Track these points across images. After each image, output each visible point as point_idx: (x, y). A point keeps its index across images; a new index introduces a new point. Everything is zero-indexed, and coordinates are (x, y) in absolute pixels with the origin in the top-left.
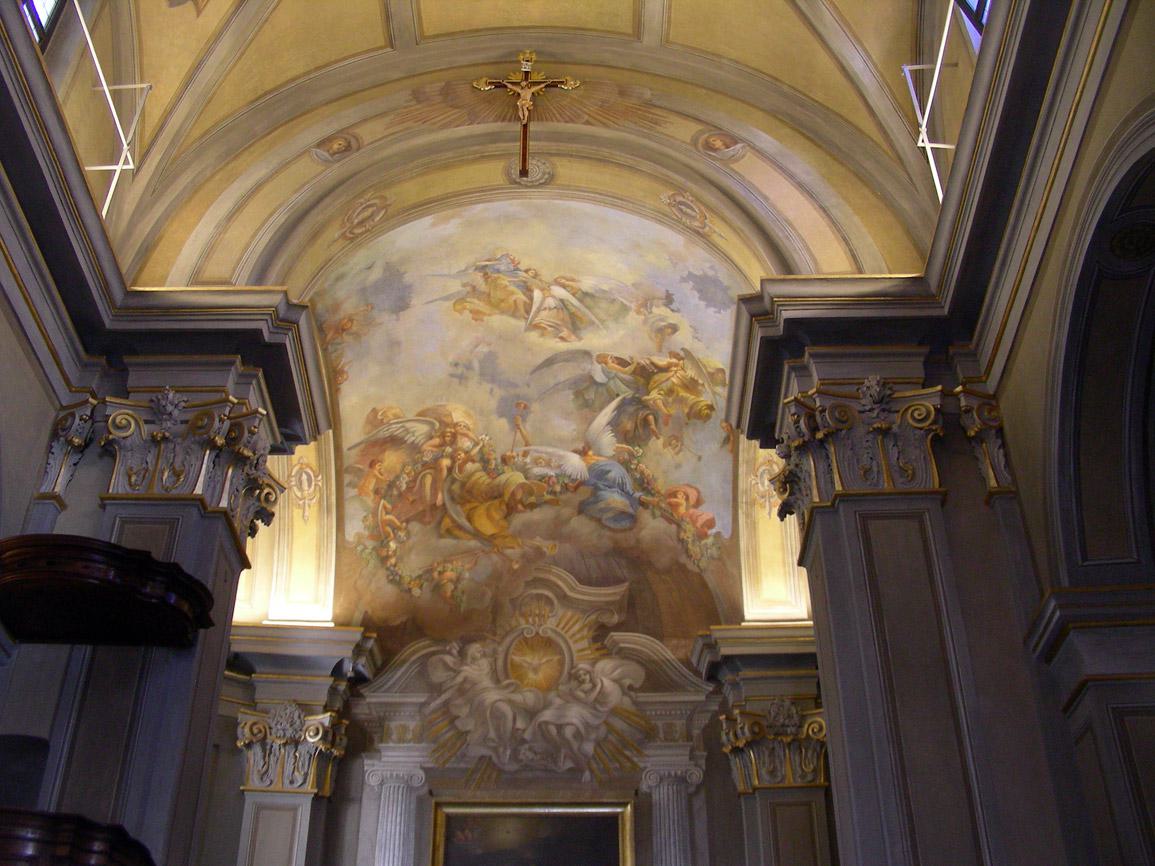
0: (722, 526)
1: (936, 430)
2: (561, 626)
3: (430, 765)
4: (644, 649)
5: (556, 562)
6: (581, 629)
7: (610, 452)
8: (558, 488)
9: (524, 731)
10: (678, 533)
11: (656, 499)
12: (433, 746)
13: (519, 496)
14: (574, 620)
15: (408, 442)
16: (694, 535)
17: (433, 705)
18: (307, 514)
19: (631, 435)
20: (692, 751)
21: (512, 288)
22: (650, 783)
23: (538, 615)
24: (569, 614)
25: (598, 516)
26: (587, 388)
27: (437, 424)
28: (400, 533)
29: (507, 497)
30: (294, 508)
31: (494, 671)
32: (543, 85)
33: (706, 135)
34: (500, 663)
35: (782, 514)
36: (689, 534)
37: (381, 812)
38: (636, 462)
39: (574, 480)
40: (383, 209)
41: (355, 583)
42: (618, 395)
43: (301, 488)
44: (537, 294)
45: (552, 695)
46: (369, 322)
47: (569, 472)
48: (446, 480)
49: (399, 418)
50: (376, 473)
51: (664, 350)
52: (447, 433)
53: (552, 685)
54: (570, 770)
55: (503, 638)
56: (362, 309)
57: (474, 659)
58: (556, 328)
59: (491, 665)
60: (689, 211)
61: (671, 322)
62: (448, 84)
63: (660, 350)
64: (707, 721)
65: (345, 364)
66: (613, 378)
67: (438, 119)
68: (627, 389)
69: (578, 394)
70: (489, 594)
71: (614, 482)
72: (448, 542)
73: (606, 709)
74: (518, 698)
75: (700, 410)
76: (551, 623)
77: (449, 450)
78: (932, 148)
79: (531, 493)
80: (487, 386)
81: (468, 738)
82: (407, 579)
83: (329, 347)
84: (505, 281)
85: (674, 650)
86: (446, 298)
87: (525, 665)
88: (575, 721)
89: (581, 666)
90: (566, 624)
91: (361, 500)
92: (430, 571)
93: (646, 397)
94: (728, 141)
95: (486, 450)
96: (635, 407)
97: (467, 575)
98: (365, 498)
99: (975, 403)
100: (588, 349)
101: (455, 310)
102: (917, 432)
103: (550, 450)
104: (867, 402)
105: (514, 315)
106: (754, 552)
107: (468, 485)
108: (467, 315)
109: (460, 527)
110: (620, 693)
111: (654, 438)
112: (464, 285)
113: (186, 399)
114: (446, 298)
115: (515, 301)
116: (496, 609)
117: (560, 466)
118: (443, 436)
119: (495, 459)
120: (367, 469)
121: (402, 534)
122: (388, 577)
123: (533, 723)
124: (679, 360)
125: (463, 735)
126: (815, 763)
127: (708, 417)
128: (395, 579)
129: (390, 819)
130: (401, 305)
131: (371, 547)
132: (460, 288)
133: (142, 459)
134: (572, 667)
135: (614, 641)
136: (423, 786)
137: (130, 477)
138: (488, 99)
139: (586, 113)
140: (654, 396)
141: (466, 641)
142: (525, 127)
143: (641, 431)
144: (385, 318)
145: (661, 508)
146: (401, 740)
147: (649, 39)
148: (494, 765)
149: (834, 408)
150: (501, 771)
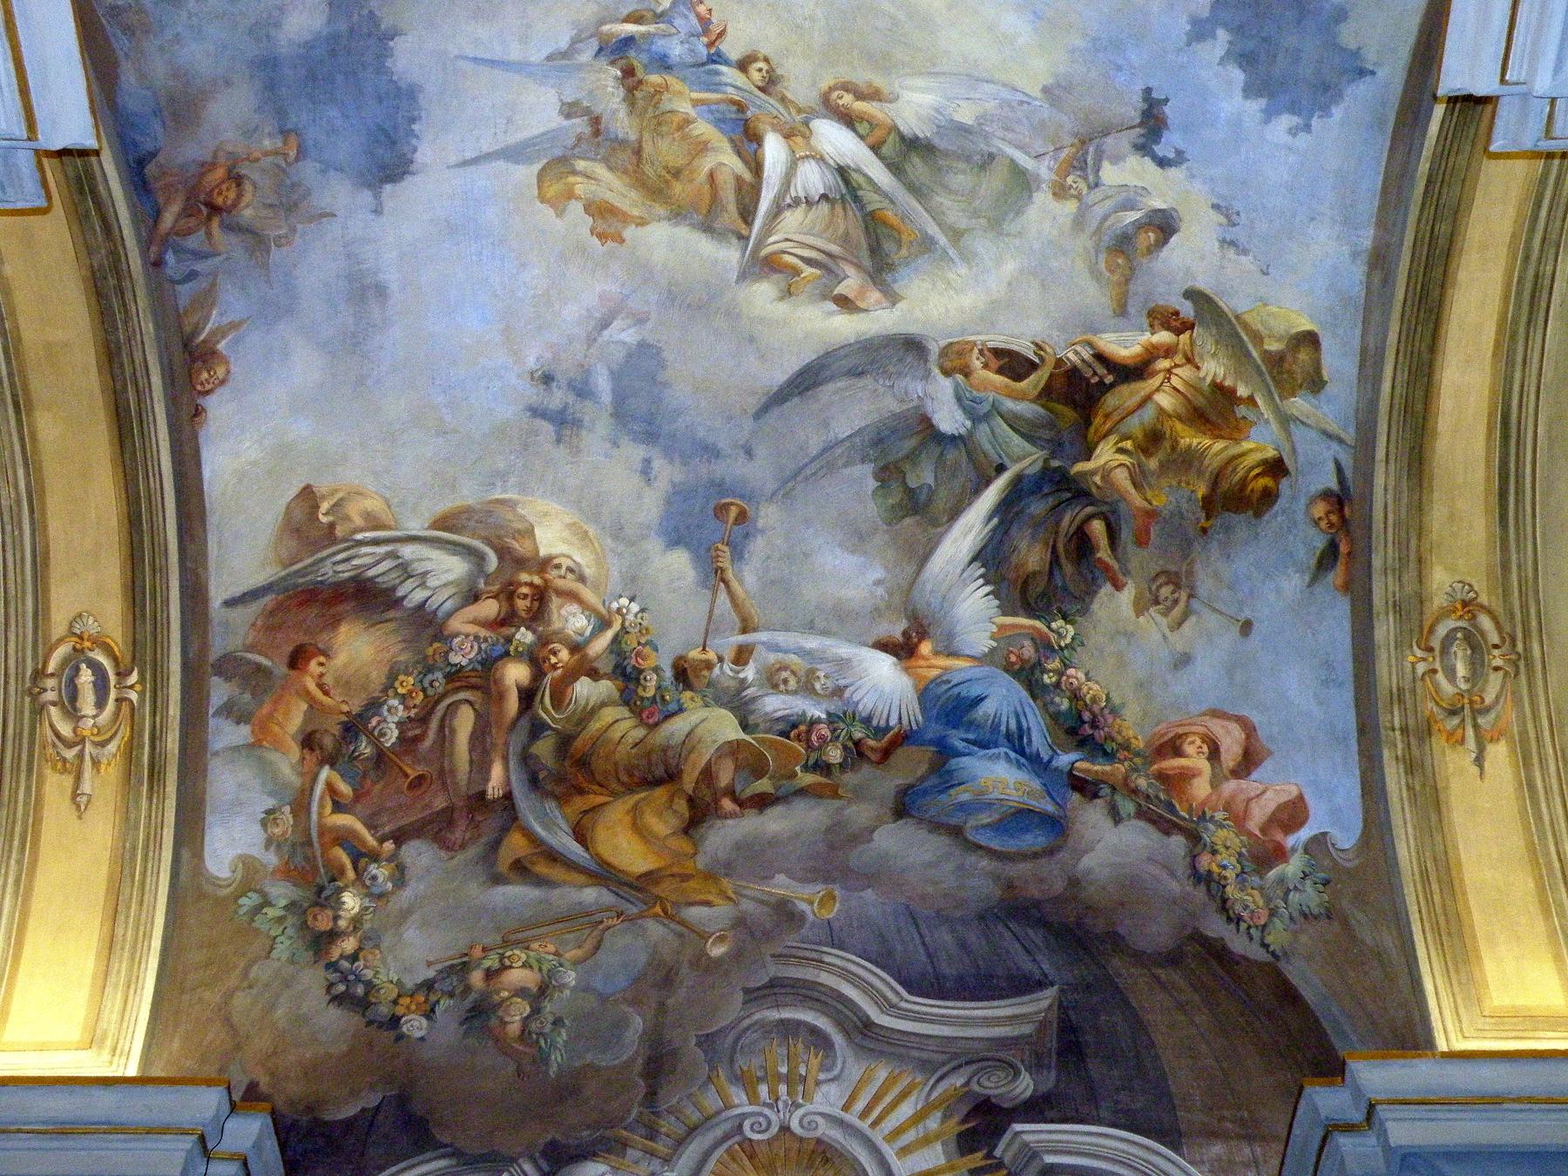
2: (860, 1105)
6: (919, 1117)
7: (979, 640)
8: (835, 755)
11: (1121, 768)
13: (725, 776)
18: (86, 787)
19: (1039, 586)
21: (703, 128)
24: (882, 1074)
25: (954, 821)
26: (912, 457)
27: (493, 561)
28: (373, 869)
29: (689, 781)
30: (48, 771)
36: (1225, 861)
38: (1055, 664)
39: (880, 731)
42: (1001, 469)
43: (72, 712)
44: (774, 150)
47: (866, 706)
50: (311, 685)
51: (1132, 310)
55: (680, 1143)
56: (267, 144)
58: (827, 265)
61: (1158, 204)
63: (1122, 310)
65: (221, 332)
69: (888, 474)
70: (638, 1023)
71: (995, 727)
72: (517, 893)
75: (1244, 482)
76: (828, 1098)
77: (525, 636)
79: (759, 771)
80: (635, 452)
83: (170, 258)
84: (682, 100)
86: (515, 154)
90: (877, 1098)
92: (462, 968)
95: (631, 642)
96: (1051, 501)
97: (570, 977)
98: (274, 757)
100: (913, 329)
101: (542, 199)
103: (812, 643)
105: (707, 228)
107: (578, 743)
108: (577, 219)
111: (1107, 588)
114: (515, 154)
115: (711, 176)
117: (838, 691)
118: (508, 593)
119: (656, 670)
120: (281, 669)
122: (330, 986)
127: (1269, 497)
131: (283, 902)
135: (1026, 1145)
143: (1068, 568)
145: (1135, 791)
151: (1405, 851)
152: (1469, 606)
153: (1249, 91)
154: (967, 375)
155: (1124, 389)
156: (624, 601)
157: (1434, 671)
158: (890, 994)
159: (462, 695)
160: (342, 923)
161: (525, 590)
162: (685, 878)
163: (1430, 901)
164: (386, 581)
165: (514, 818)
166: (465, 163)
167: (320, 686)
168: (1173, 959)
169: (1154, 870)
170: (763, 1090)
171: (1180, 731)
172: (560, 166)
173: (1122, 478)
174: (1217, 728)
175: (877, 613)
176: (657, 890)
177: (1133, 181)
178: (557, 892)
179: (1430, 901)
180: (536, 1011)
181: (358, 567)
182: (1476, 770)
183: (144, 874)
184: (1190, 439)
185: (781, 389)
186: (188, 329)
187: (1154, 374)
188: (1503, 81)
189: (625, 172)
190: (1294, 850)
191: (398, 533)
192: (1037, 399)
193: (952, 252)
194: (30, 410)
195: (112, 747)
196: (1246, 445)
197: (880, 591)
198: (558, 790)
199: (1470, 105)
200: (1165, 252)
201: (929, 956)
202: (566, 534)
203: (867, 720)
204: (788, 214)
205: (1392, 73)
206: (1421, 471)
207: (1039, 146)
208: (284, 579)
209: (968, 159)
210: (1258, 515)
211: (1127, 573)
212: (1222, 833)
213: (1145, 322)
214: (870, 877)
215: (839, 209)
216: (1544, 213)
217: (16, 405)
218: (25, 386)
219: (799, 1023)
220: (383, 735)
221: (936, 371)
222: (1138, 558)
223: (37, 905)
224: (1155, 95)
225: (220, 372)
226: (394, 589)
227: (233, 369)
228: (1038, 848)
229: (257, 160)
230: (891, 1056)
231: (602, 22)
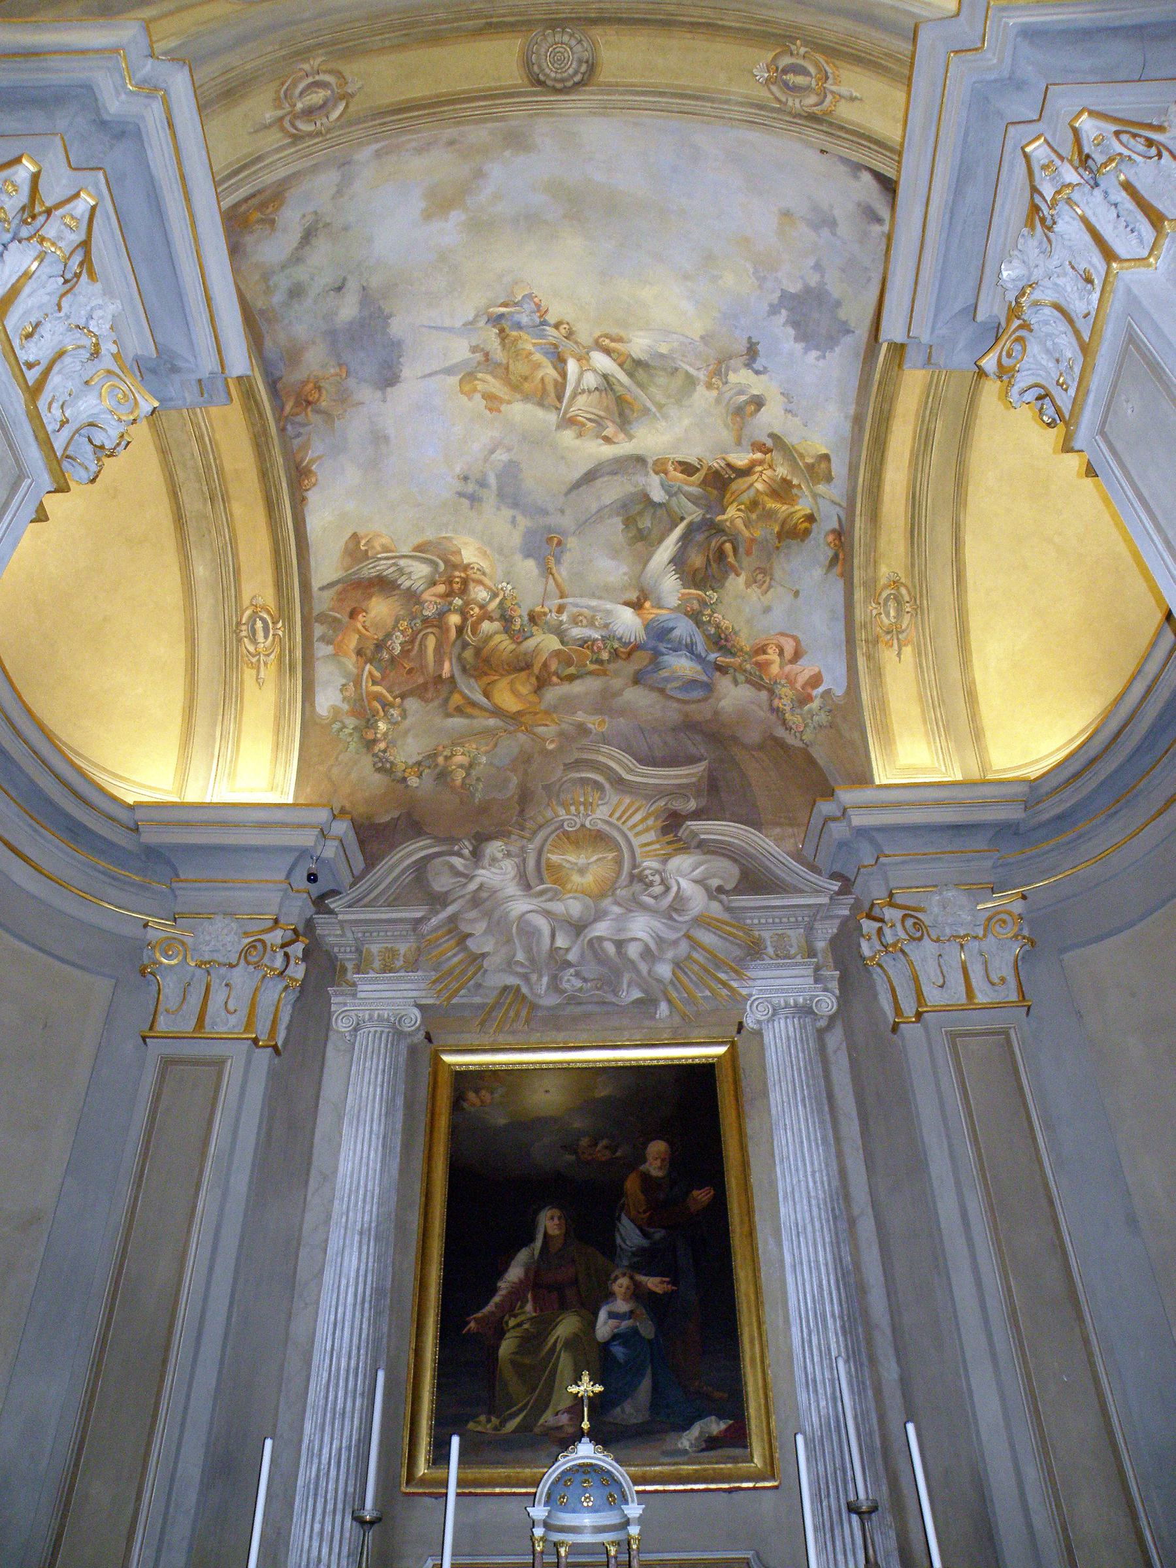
5: (605, 740)
6: (644, 819)
7: (673, 600)
8: (605, 656)
9: (568, 950)
11: (739, 660)
12: (434, 975)
13: (553, 666)
18: (262, 675)
19: (699, 576)
20: (817, 969)
21: (538, 357)
22: (759, 1016)
26: (641, 513)
27: (442, 566)
28: (392, 711)
29: (536, 669)
30: (245, 668)
34: (531, 863)
36: (785, 704)
38: (708, 612)
39: (625, 644)
41: (329, 770)
42: (682, 519)
43: (254, 641)
44: (572, 366)
45: (607, 903)
47: (619, 633)
49: (390, 551)
50: (360, 627)
51: (743, 442)
53: (606, 890)
54: (638, 1002)
55: (534, 833)
56: (332, 371)
57: (494, 860)
58: (598, 422)
61: (756, 392)
63: (739, 443)
64: (835, 931)
65: (313, 461)
66: (676, 494)
69: (629, 522)
70: (515, 780)
72: (457, 722)
73: (687, 918)
74: (557, 907)
75: (796, 524)
76: (602, 812)
77: (458, 602)
79: (569, 663)
80: (507, 513)
83: (289, 427)
84: (528, 343)
85: (778, 841)
86: (449, 371)
87: (568, 865)
90: (624, 812)
91: (339, 662)
92: (434, 756)
93: (720, 518)
95: (508, 604)
96: (706, 534)
97: (484, 760)
98: (344, 660)
100: (640, 452)
101: (462, 392)
103: (594, 603)
105: (541, 404)
106: (882, 705)
108: (478, 401)
109: (473, 704)
110: (706, 898)
112: (474, 349)
114: (449, 371)
115: (542, 379)
116: (525, 798)
117: (606, 626)
118: (450, 582)
119: (520, 616)
120: (345, 619)
121: (395, 712)
123: (581, 938)
124: (765, 454)
125: (477, 959)
127: (807, 532)
128: (384, 768)
129: (366, 1079)
130: (388, 378)
132: (469, 355)
134: (634, 866)
135: (692, 831)
136: (418, 1029)
141: (481, 839)
143: (714, 565)
144: (366, 394)
145: (745, 671)
146: (387, 968)
148: (524, 997)
150: (534, 1007)
151: (865, 696)
152: (896, 583)
153: (796, 339)
154: (666, 474)
155: (740, 481)
156: (504, 584)
157: (880, 614)
158: (631, 766)
159: (429, 630)
160: (379, 736)
161: (457, 580)
162: (536, 714)
163: (875, 719)
165: (456, 687)
166: (425, 376)
167: (364, 627)
168: (761, 747)
169: (754, 707)
170: (573, 808)
171: (766, 642)
173: (739, 522)
174: (783, 641)
175: (624, 588)
176: (523, 719)
177: (744, 381)
178: (475, 721)
179: (875, 719)
180: (468, 774)
181: (378, 571)
182: (897, 659)
183: (290, 713)
184: (771, 504)
185: (577, 482)
186: (298, 459)
187: (755, 473)
188: (908, 336)
189: (502, 379)
190: (816, 697)
191: (394, 554)
192: (699, 486)
193: (658, 415)
194: (229, 502)
195: (272, 656)
196: (797, 508)
197: (626, 578)
198: (476, 673)
199: (898, 350)
200: (759, 415)
201: (650, 748)
202: (476, 552)
203: (620, 639)
204: (579, 397)
205: (862, 332)
206: (876, 521)
207: (698, 364)
208: (346, 576)
209: (665, 370)
210: (802, 541)
211: (742, 568)
212: (784, 689)
213: (750, 448)
214: (622, 712)
215: (604, 395)
216: (930, 400)
217: (223, 499)
218: (226, 489)
219: (589, 779)
220: (393, 649)
221: (651, 472)
222: (746, 561)
223: (244, 728)
224: (753, 340)
225: (313, 480)
226: (396, 580)
227: (320, 478)
228: (700, 698)
229: (328, 378)
230: (631, 793)
231: (489, 307)
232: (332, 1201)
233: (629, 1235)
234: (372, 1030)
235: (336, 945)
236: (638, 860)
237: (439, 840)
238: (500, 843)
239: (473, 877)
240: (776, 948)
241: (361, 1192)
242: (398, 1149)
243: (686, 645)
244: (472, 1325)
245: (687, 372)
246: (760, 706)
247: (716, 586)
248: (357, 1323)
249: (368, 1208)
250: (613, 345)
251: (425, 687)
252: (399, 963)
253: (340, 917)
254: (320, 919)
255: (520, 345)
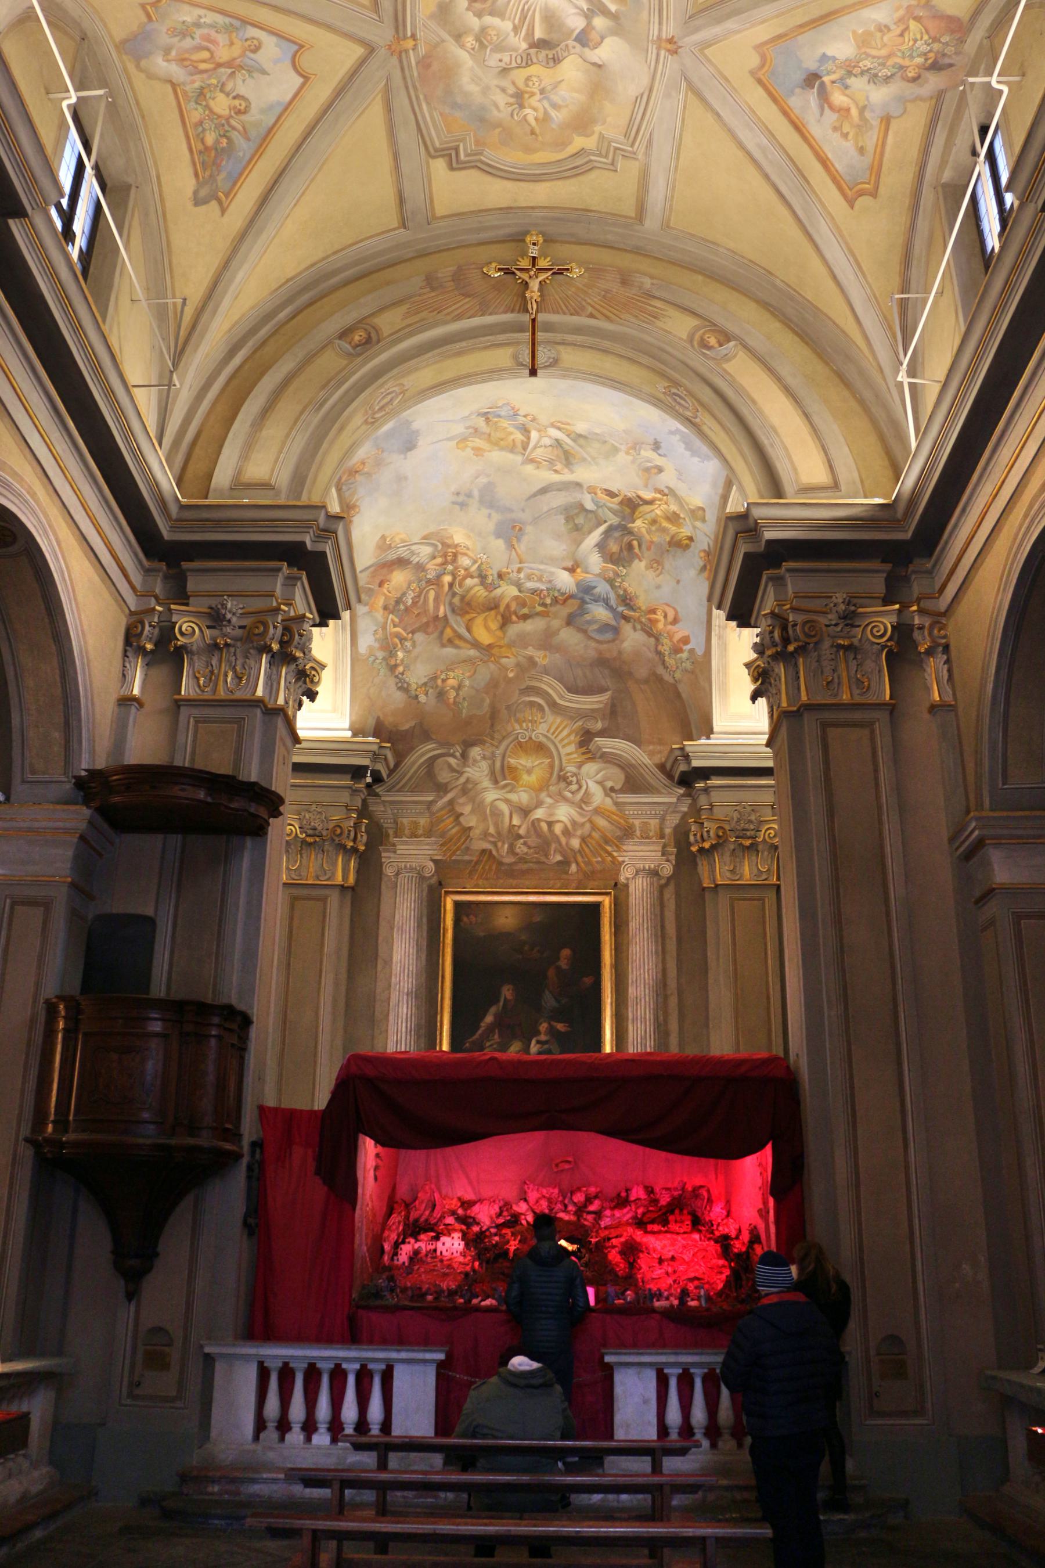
0: (697, 644)
1: (891, 646)
3: (439, 858)
4: (625, 754)
5: (546, 671)
6: (569, 735)
8: (548, 601)
9: (519, 827)
10: (656, 646)
11: (637, 615)
12: (441, 841)
14: (563, 725)
15: (414, 562)
16: (670, 649)
17: (440, 804)
19: (616, 557)
20: (664, 846)
21: (511, 429)
23: (530, 721)
25: (584, 628)
26: (577, 515)
27: (440, 546)
28: (406, 643)
29: (502, 608)
31: (493, 774)
32: (550, 273)
33: (702, 331)
34: (498, 764)
35: (754, 698)
36: (666, 648)
37: (398, 899)
38: (619, 580)
39: (563, 594)
40: (400, 393)
42: (605, 522)
44: (534, 435)
46: (379, 463)
47: (558, 587)
48: (447, 594)
50: (385, 591)
52: (449, 554)
53: (543, 786)
54: (559, 862)
55: (500, 742)
58: (551, 462)
59: (490, 766)
60: (682, 402)
61: (658, 464)
62: (460, 268)
63: (646, 486)
67: (454, 307)
68: (614, 517)
69: (569, 519)
70: (488, 701)
71: (599, 596)
72: (449, 651)
73: (590, 808)
74: (513, 797)
75: (681, 540)
76: (542, 728)
77: (450, 567)
78: (909, 383)
79: (524, 605)
80: (485, 511)
81: (471, 835)
82: (414, 686)
84: (504, 423)
85: (651, 754)
86: (449, 439)
87: (520, 767)
88: (563, 819)
89: (568, 769)
90: (557, 729)
92: (434, 678)
93: (630, 525)
94: (722, 338)
95: (484, 567)
96: (621, 533)
97: (467, 683)
99: (927, 622)
102: (875, 646)
103: (542, 567)
104: (833, 617)
109: (460, 637)
110: (603, 795)
113: (241, 606)
114: (449, 439)
116: (494, 715)
118: (445, 556)
119: (492, 575)
122: (397, 684)
126: (769, 863)
127: (687, 546)
133: (207, 662)
136: (433, 875)
137: (198, 679)
138: (497, 286)
139: (590, 304)
140: (639, 525)
141: (468, 745)
142: (534, 320)
143: (625, 553)
145: (641, 622)
146: (414, 835)
147: (651, 223)
148: (494, 857)
149: (805, 623)
150: (500, 863)
164: (407, 557)
168: (646, 681)
170: (524, 725)
172: (465, 439)
178: (461, 651)
180: (458, 694)
184: (665, 524)
203: (559, 591)
210: (685, 550)
219: (535, 702)
221: (585, 492)
222: (647, 554)
225: (357, 510)
232: (391, 977)
233: (549, 1000)
234: (407, 875)
235: (382, 818)
236: (564, 765)
237: (442, 745)
238: (478, 749)
239: (463, 773)
240: (641, 831)
241: (406, 971)
242: (425, 947)
243: (604, 599)
244: (467, 1045)
245: (613, 444)
246: (649, 649)
247: (626, 564)
248: (408, 1041)
249: (410, 980)
250: (563, 426)
251: (427, 624)
252: (420, 832)
253: (383, 798)
254: (371, 800)
255: (499, 424)
